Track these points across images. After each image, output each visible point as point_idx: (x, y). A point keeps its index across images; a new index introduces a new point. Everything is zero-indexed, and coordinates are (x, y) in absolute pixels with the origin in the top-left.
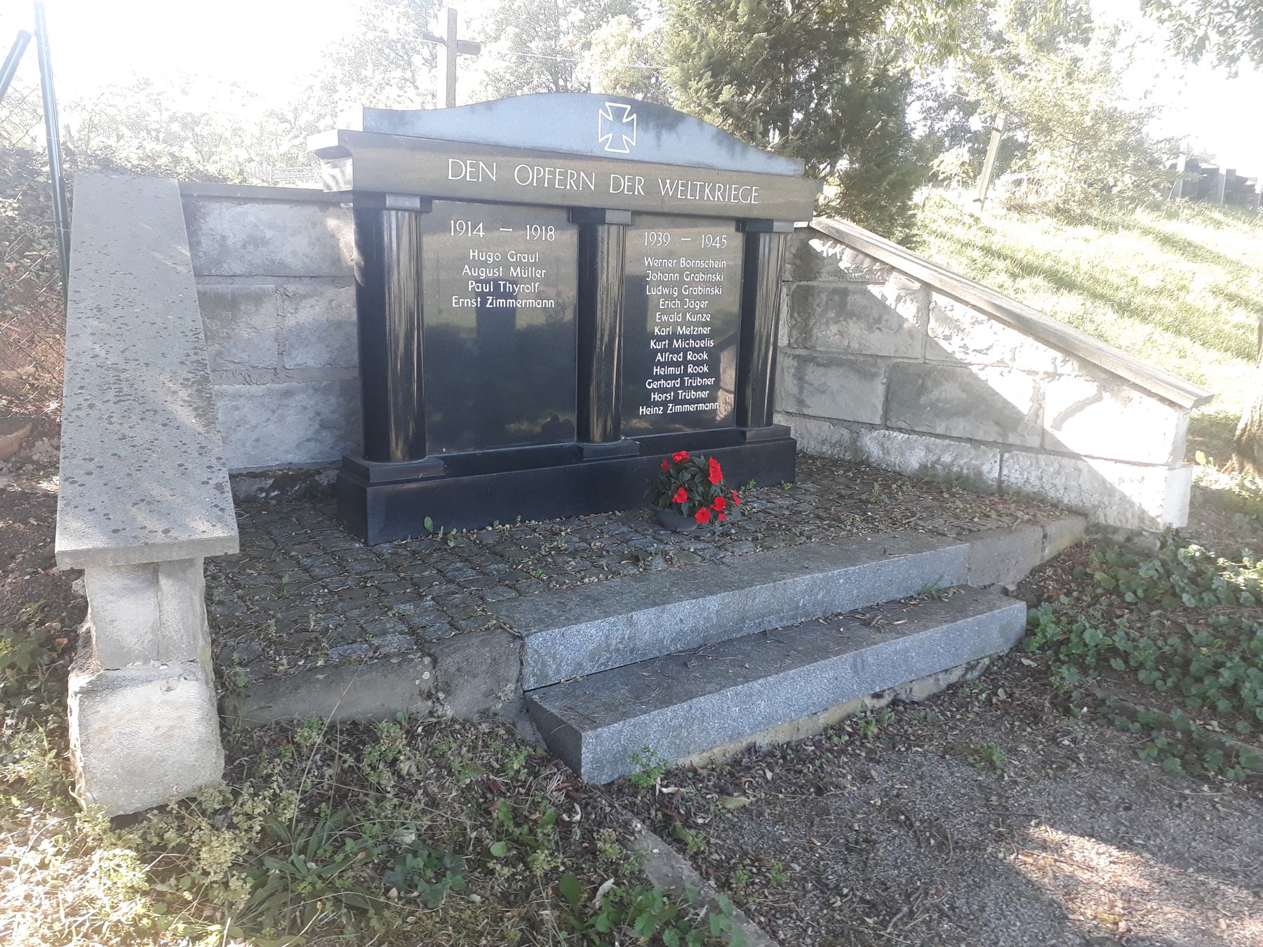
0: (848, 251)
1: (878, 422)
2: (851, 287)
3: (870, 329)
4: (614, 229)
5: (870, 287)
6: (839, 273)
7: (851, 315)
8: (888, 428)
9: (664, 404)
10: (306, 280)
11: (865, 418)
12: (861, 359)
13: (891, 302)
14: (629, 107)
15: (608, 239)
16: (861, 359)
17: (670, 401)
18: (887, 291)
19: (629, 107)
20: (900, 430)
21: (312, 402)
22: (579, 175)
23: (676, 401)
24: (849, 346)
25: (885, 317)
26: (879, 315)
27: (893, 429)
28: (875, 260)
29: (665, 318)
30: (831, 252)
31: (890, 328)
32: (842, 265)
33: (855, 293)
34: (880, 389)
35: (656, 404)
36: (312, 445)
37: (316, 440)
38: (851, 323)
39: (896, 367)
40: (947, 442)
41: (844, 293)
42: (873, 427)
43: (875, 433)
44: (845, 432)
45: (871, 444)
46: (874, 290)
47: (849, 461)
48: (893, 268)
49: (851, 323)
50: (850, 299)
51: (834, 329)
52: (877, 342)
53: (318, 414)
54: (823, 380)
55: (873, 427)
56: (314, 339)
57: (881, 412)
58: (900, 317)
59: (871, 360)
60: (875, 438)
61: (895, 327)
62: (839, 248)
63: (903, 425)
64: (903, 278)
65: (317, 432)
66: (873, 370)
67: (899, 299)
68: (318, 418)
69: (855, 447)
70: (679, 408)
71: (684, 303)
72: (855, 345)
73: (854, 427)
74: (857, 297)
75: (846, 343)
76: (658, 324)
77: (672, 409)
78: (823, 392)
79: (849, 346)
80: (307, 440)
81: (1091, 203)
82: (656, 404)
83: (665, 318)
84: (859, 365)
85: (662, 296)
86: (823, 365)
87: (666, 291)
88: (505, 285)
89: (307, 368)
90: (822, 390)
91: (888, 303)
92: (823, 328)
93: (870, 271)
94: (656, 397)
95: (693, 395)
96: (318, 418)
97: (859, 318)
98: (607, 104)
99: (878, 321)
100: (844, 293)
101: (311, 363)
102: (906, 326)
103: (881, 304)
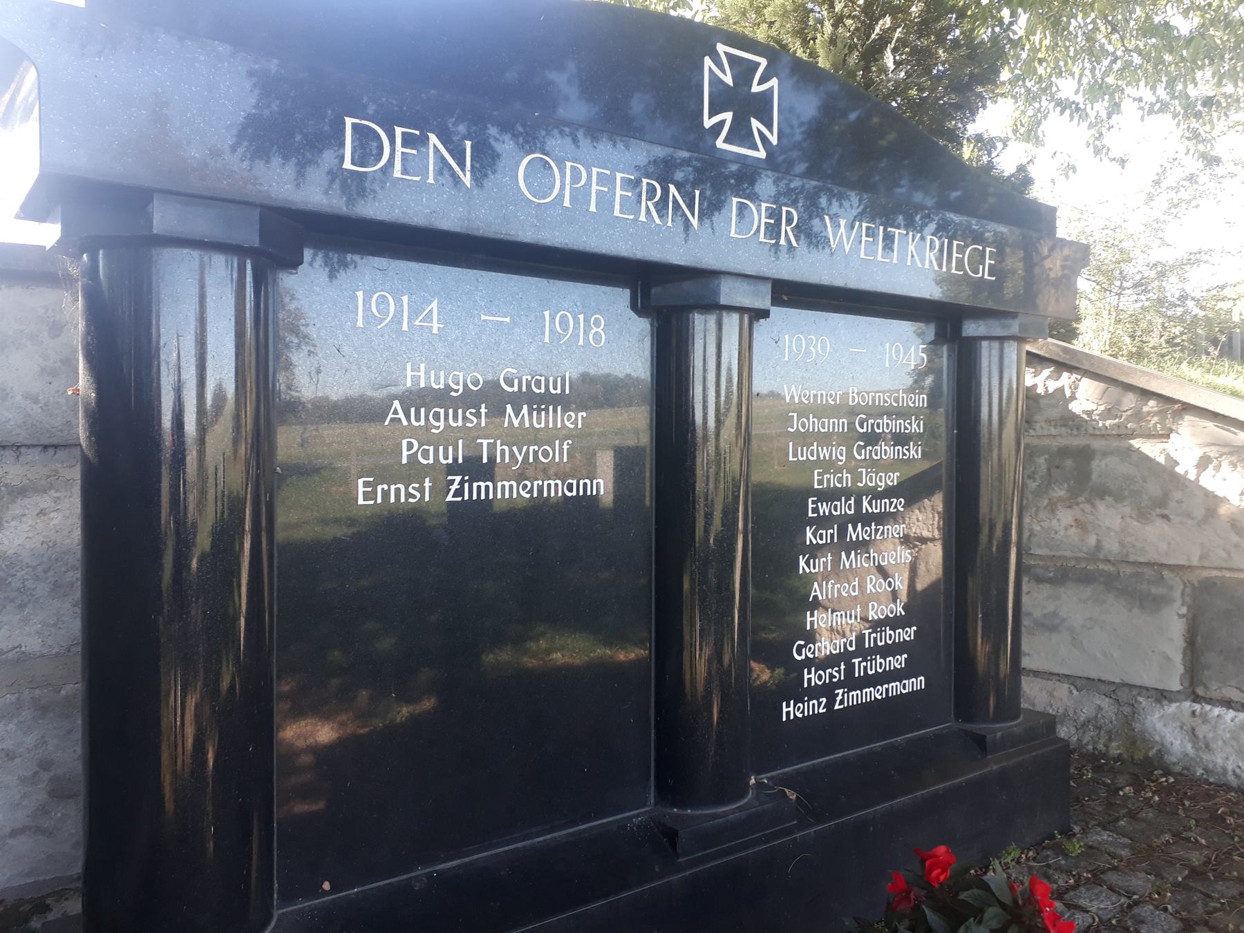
0: (1086, 382)
1: (1175, 685)
2: (1096, 444)
3: (1143, 516)
4: (732, 322)
5: (1136, 443)
6: (1073, 422)
7: (1102, 492)
8: (1197, 699)
9: (828, 691)
10: (34, 455)
11: (1148, 677)
12: (1129, 570)
13: (1186, 467)
14: (763, 62)
15: (713, 345)
16: (1129, 570)
17: (840, 684)
18: (1183, 448)
19: (763, 62)
20: (1228, 704)
21: (30, 740)
22: (666, 191)
23: (852, 683)
24: (1098, 547)
25: (1177, 495)
26: (1163, 492)
27: (1210, 701)
28: (1146, 394)
29: (824, 509)
30: (1053, 386)
31: (1189, 516)
32: (1076, 407)
33: (1105, 454)
34: (1177, 629)
35: (814, 692)
36: (22, 844)
37: (38, 830)
38: (1101, 506)
39: (1207, 587)
40: (262, 482)
41: (1084, 455)
42: (1162, 696)
43: (1172, 708)
44: (1105, 703)
45: (1167, 729)
46: (1150, 449)
47: (1119, 758)
48: (1188, 408)
49: (1101, 506)
50: (1097, 465)
51: (1065, 517)
52: (1157, 540)
53: (45, 765)
54: (1051, 607)
55: (1162, 696)
56: (42, 589)
57: (1179, 668)
58: (1208, 494)
59: (1148, 572)
60: (1174, 717)
61: (1199, 513)
62: (1066, 379)
63: (1235, 695)
64: (1210, 425)
65: (43, 810)
66: (1155, 590)
67: (1204, 462)
68: (45, 776)
69: (1135, 739)
70: (856, 697)
71: (857, 477)
72: (1112, 546)
73: (1123, 695)
74: (1112, 463)
75: (1092, 540)
76: (811, 522)
77: (847, 699)
78: (1053, 629)
79: (1098, 547)
80: (14, 834)
81: (1216, 346)
82: (814, 692)
83: (824, 509)
84: (1135, 583)
85: (818, 463)
86: (1050, 581)
87: (824, 453)
88: (492, 447)
89: (23, 659)
90: (1050, 625)
91: (1179, 470)
92: (1043, 515)
93: (1138, 416)
94: (811, 677)
95: (879, 665)
96: (45, 776)
97: (1119, 498)
98: (721, 48)
99: (1162, 502)
100: (1084, 455)
101: (33, 644)
102: (1223, 510)
103: (1167, 474)
